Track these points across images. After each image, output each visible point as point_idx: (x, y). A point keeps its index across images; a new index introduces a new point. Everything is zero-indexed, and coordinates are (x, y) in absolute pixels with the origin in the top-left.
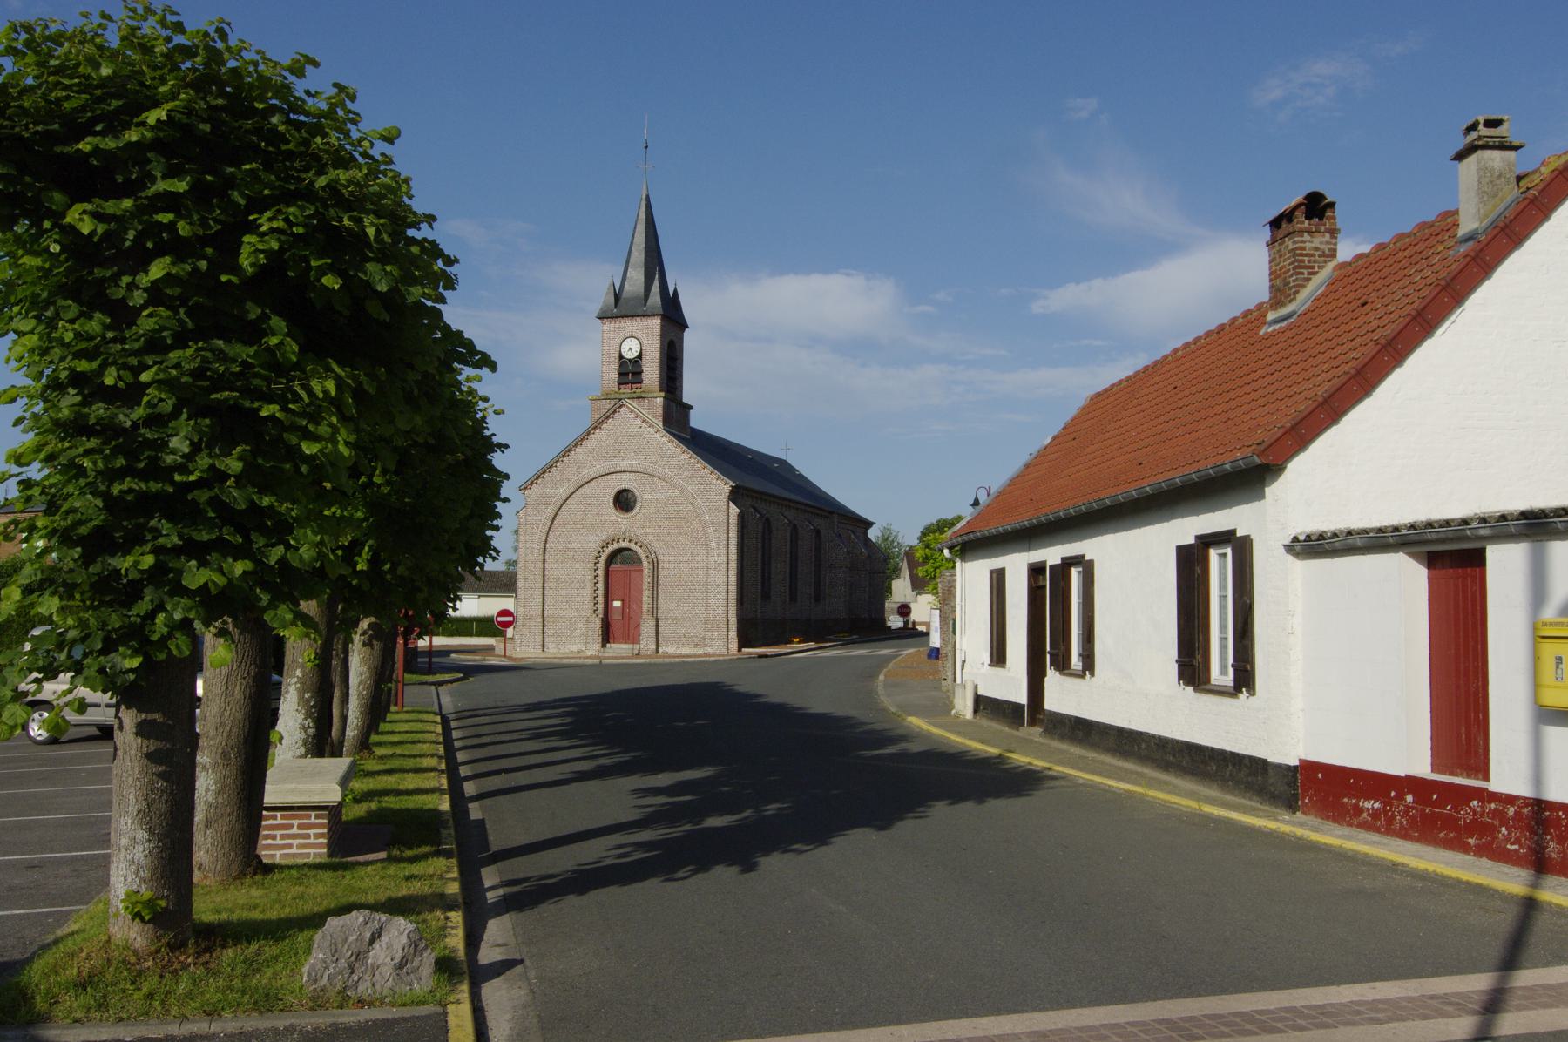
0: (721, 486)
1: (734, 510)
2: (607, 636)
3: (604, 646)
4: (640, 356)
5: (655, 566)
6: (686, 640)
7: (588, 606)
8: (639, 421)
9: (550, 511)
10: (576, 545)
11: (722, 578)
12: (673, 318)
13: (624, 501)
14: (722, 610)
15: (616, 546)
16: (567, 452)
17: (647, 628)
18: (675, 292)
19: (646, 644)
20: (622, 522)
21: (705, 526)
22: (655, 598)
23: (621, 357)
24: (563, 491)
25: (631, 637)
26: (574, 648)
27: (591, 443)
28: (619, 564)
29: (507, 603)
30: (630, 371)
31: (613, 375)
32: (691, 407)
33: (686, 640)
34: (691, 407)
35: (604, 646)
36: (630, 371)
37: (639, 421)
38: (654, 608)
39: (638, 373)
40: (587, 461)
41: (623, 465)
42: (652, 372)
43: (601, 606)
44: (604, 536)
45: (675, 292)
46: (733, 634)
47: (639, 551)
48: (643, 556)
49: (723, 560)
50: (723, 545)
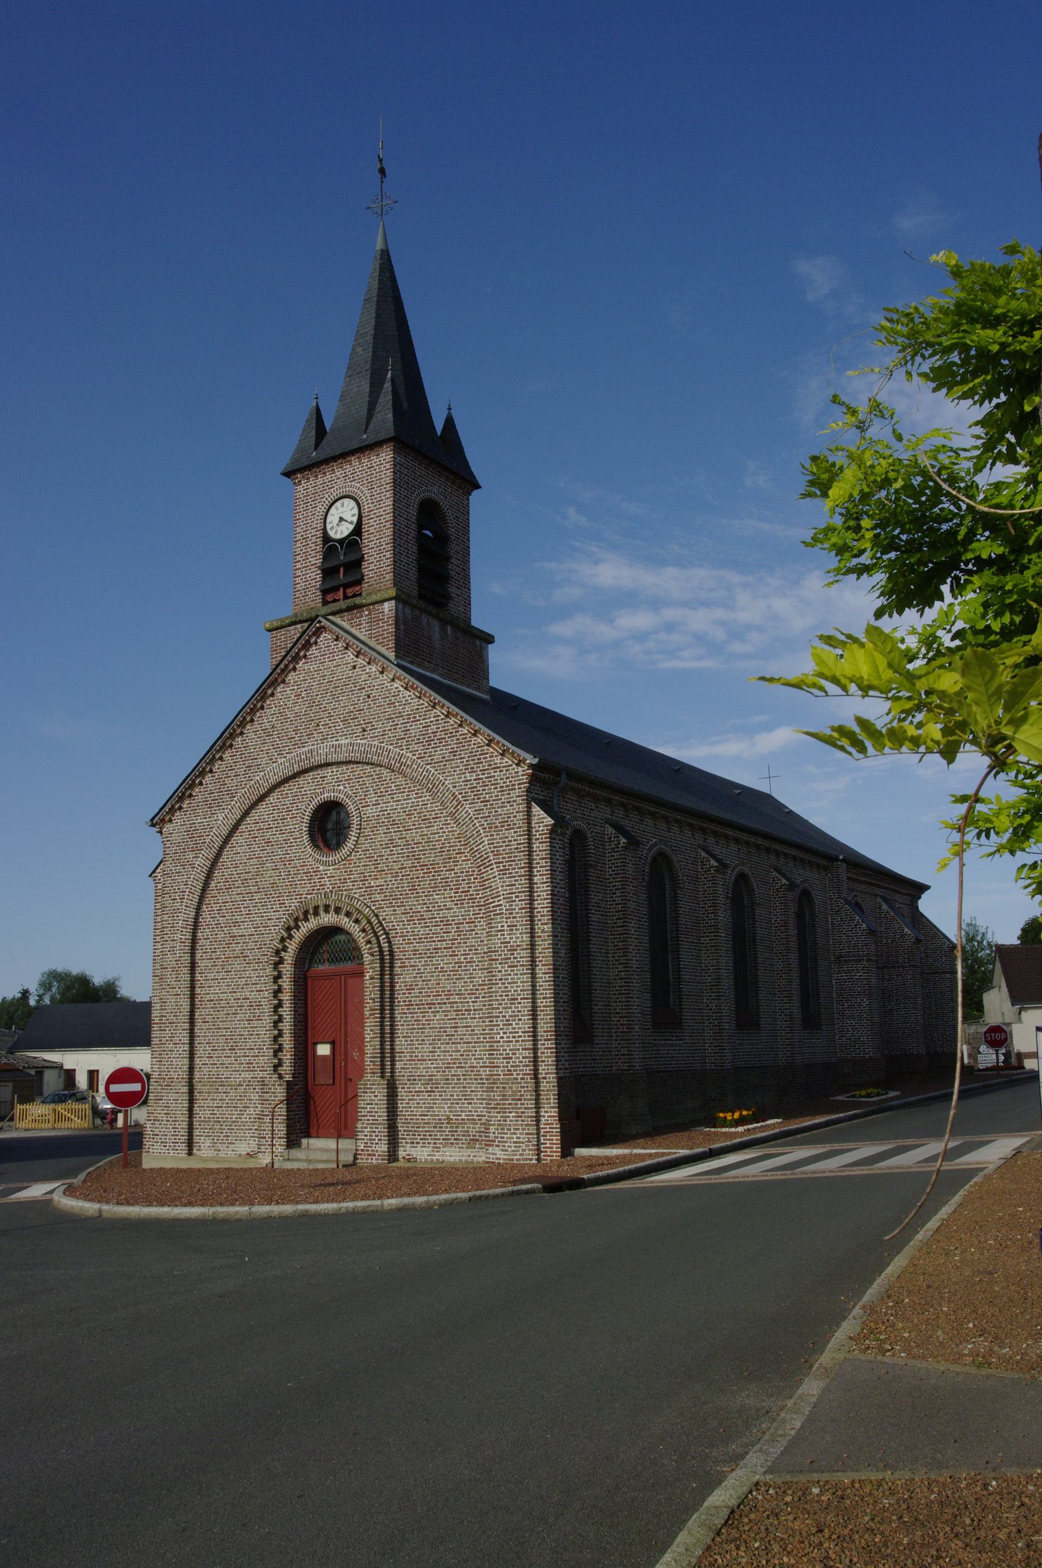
0: (511, 770)
1: (542, 820)
2: (302, 1120)
3: (292, 1142)
4: (358, 530)
5: (387, 961)
6: (450, 1129)
7: (266, 1059)
8: (350, 656)
9: (202, 861)
10: (246, 929)
11: (520, 981)
12: (434, 459)
13: (328, 825)
14: (523, 1056)
15: (313, 924)
16: (226, 740)
17: (371, 1100)
18: (449, 422)
19: (369, 1141)
20: (326, 873)
21: (482, 864)
22: (388, 1035)
23: (326, 538)
24: (222, 821)
25: (344, 1128)
26: (243, 1148)
27: (267, 717)
28: (324, 969)
29: (138, 1059)
30: (341, 563)
31: (310, 575)
32: (489, 639)
33: (450, 1129)
34: (489, 639)
35: (292, 1142)
36: (341, 563)
37: (350, 656)
38: (387, 1056)
39: (356, 564)
40: (263, 756)
41: (323, 751)
42: (379, 562)
43: (287, 1057)
44: (391, 918)
45: (449, 422)
46: (550, 1113)
47: (354, 929)
48: (361, 939)
49: (521, 937)
50: (519, 905)
